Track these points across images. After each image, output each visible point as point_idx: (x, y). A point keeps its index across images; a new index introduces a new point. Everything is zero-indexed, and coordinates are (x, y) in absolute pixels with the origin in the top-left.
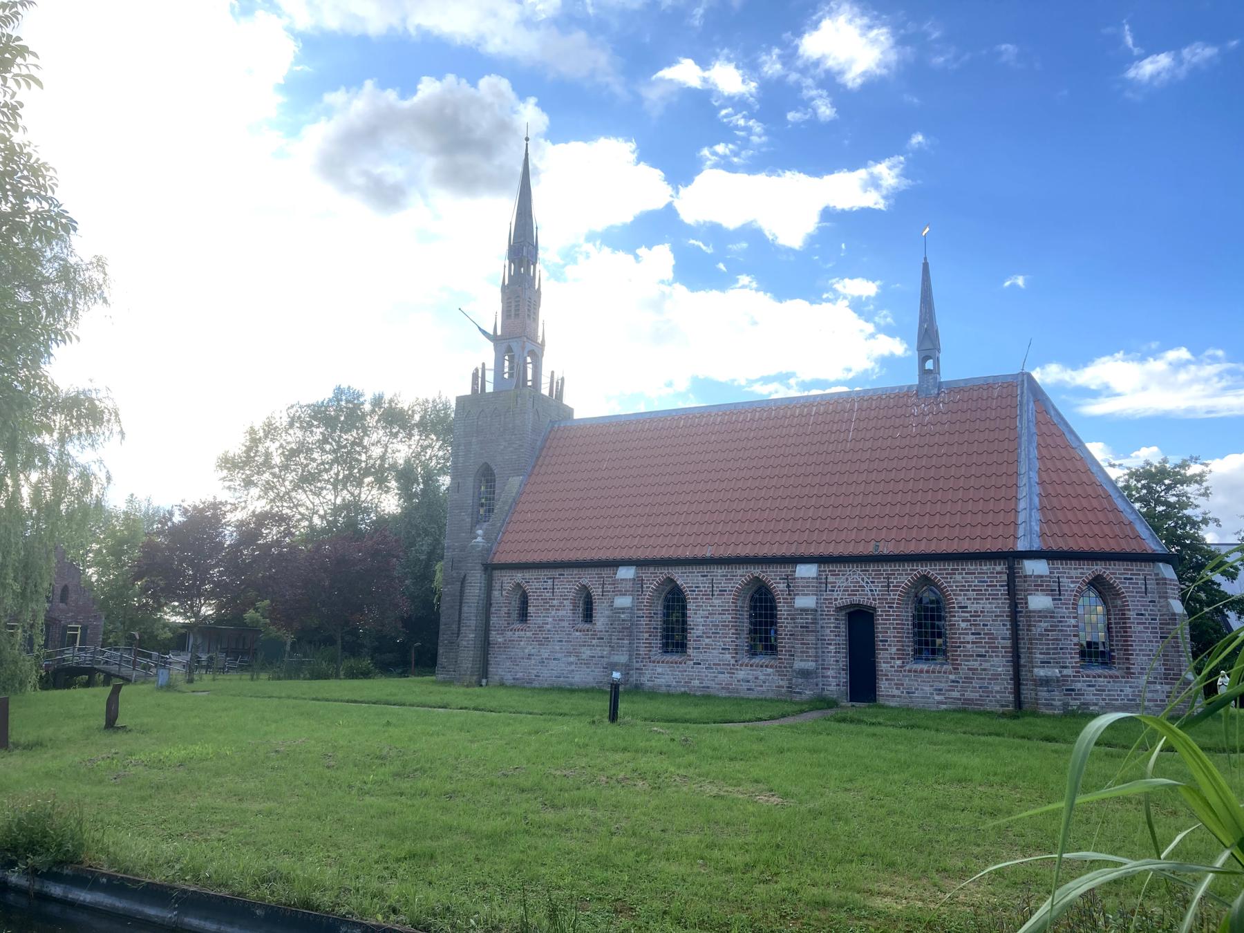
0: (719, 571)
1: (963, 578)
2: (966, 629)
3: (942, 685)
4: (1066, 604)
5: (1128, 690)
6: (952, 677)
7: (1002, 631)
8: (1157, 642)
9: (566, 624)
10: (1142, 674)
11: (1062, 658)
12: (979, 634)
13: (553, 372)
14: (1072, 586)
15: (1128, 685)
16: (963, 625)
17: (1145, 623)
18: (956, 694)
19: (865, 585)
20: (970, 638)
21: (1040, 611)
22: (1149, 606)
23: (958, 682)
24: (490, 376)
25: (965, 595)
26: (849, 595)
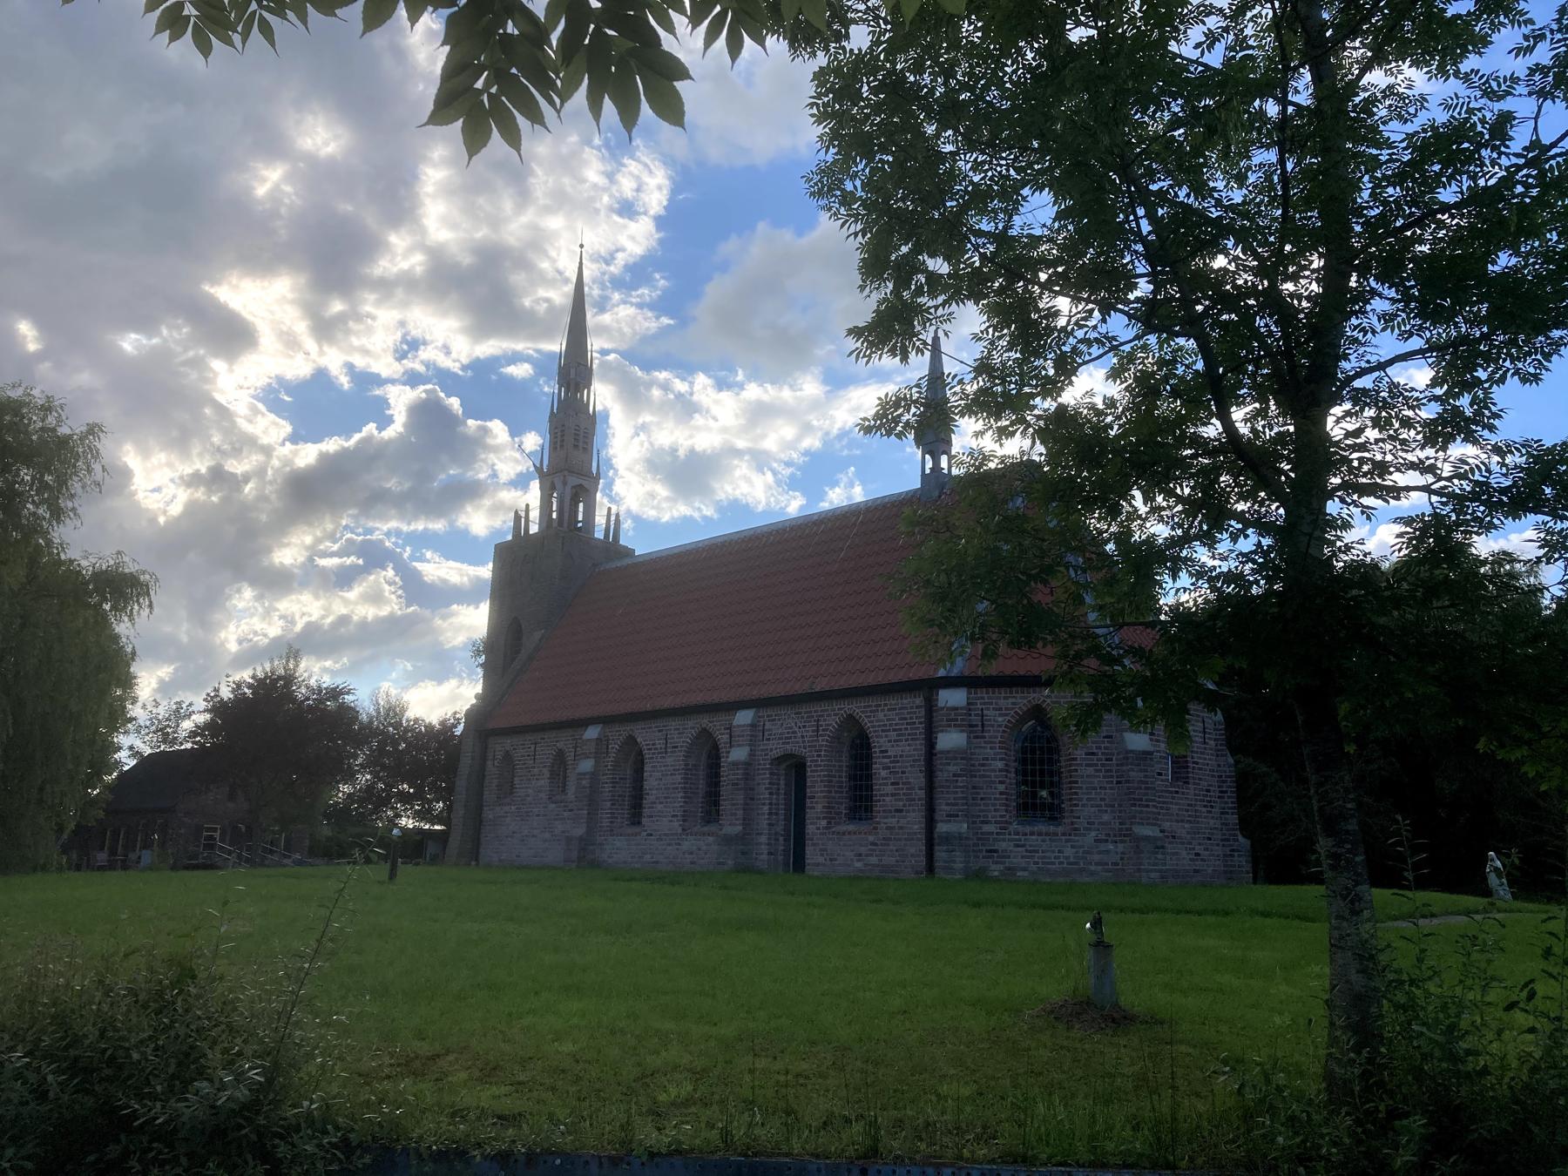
0: (673, 724)
1: (885, 716)
2: (886, 779)
3: (863, 850)
4: (991, 742)
5: (1069, 852)
6: (871, 838)
7: (917, 779)
8: (1111, 788)
9: (543, 795)
10: (1090, 829)
11: (984, 811)
12: (898, 784)
14: (1000, 719)
15: (1069, 844)
16: (884, 773)
17: (1096, 765)
18: (874, 860)
19: (797, 730)
20: (890, 789)
21: (948, 752)
22: (1104, 742)
23: (876, 844)
24: (535, 514)
25: (886, 736)
26: (783, 743)
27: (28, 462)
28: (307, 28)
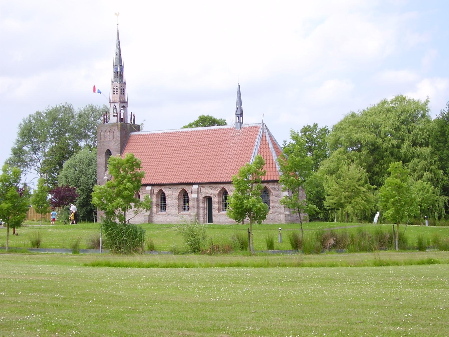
13: (131, 113)
27: (25, 122)
28: (119, 54)
